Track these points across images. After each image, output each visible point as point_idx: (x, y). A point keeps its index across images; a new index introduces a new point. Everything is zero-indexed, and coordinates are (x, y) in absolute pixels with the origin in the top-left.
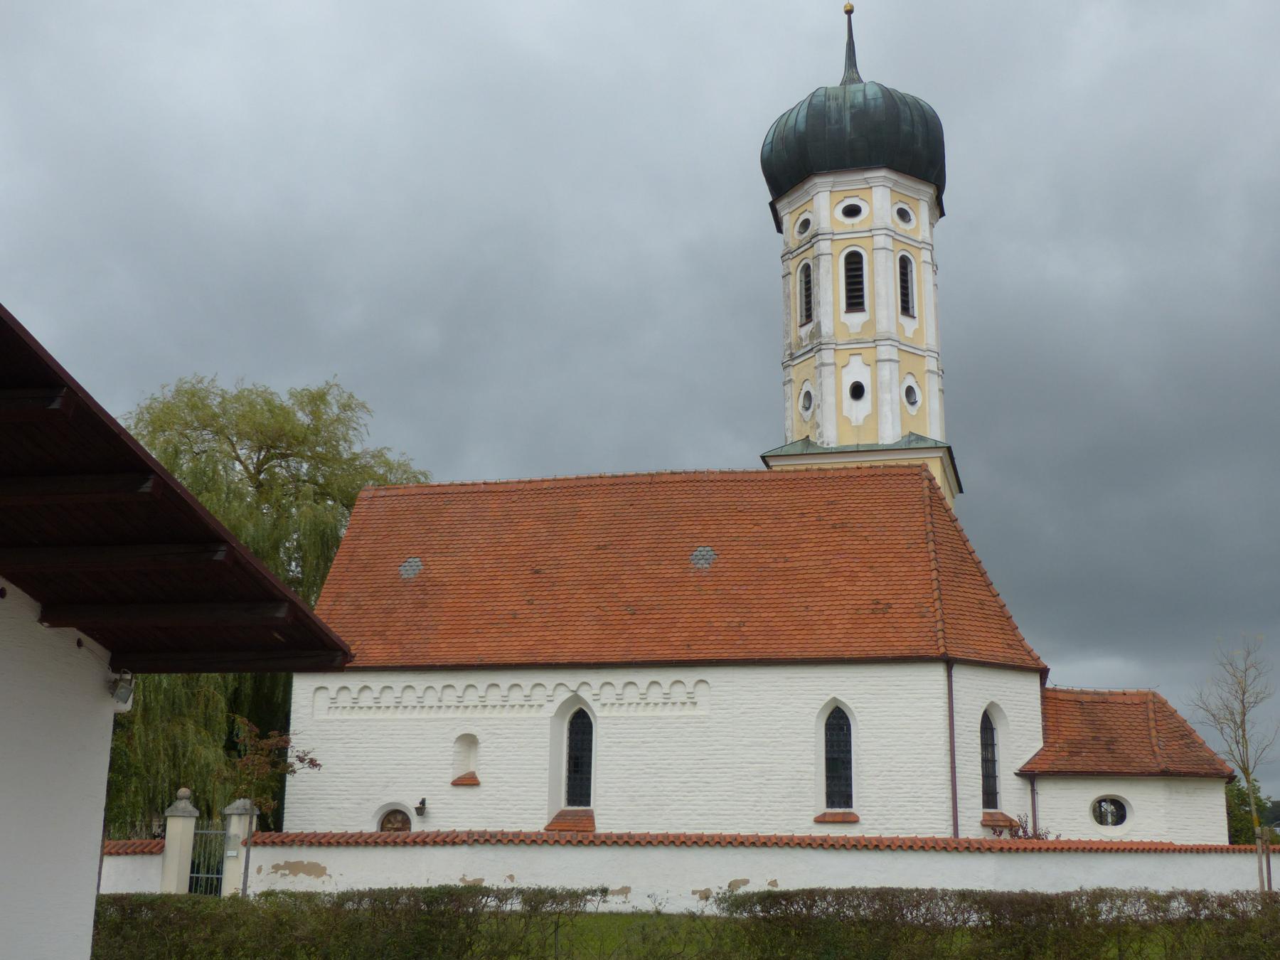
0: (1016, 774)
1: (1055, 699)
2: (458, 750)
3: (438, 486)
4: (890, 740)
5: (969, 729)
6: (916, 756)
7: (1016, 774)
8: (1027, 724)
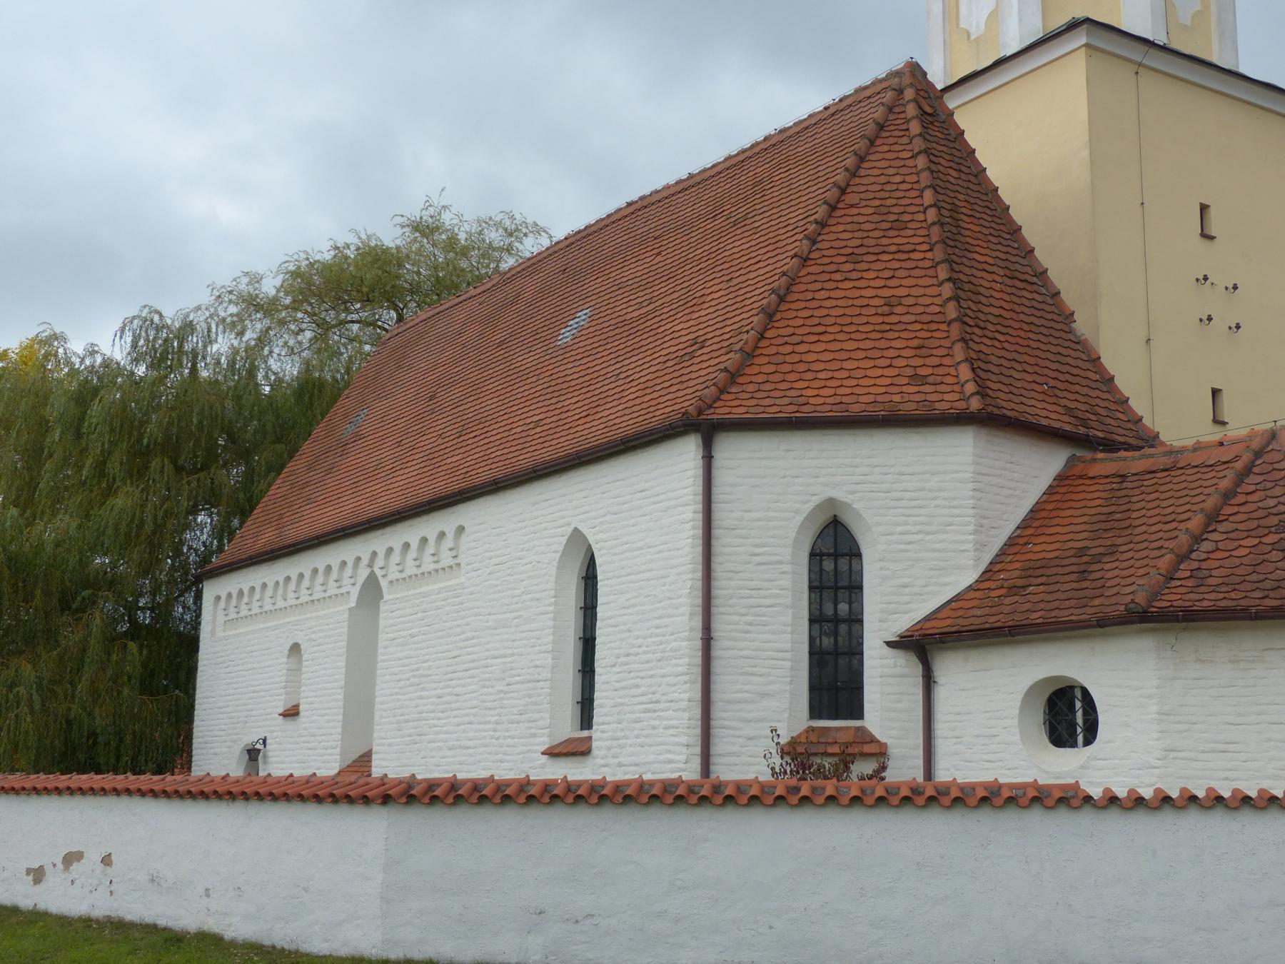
0: (890, 644)
1: (1081, 477)
2: (899, 671)
3: (770, 315)
4: (628, 596)
5: (758, 559)
6: (657, 622)
7: (889, 644)
8: (929, 538)
